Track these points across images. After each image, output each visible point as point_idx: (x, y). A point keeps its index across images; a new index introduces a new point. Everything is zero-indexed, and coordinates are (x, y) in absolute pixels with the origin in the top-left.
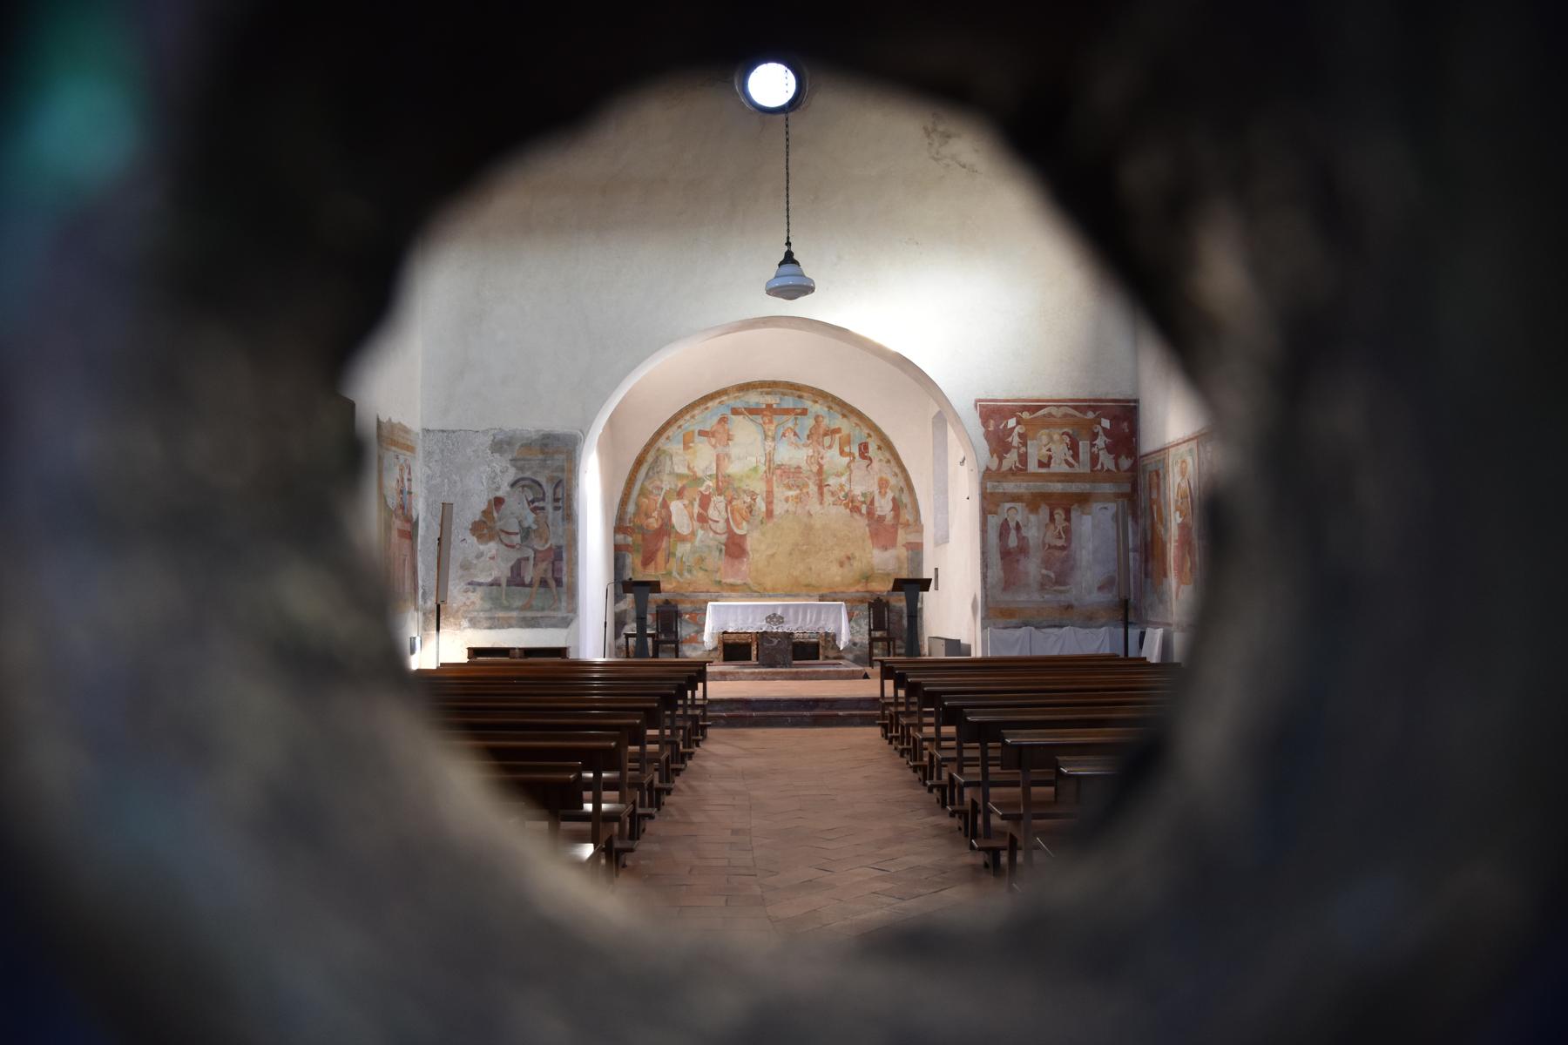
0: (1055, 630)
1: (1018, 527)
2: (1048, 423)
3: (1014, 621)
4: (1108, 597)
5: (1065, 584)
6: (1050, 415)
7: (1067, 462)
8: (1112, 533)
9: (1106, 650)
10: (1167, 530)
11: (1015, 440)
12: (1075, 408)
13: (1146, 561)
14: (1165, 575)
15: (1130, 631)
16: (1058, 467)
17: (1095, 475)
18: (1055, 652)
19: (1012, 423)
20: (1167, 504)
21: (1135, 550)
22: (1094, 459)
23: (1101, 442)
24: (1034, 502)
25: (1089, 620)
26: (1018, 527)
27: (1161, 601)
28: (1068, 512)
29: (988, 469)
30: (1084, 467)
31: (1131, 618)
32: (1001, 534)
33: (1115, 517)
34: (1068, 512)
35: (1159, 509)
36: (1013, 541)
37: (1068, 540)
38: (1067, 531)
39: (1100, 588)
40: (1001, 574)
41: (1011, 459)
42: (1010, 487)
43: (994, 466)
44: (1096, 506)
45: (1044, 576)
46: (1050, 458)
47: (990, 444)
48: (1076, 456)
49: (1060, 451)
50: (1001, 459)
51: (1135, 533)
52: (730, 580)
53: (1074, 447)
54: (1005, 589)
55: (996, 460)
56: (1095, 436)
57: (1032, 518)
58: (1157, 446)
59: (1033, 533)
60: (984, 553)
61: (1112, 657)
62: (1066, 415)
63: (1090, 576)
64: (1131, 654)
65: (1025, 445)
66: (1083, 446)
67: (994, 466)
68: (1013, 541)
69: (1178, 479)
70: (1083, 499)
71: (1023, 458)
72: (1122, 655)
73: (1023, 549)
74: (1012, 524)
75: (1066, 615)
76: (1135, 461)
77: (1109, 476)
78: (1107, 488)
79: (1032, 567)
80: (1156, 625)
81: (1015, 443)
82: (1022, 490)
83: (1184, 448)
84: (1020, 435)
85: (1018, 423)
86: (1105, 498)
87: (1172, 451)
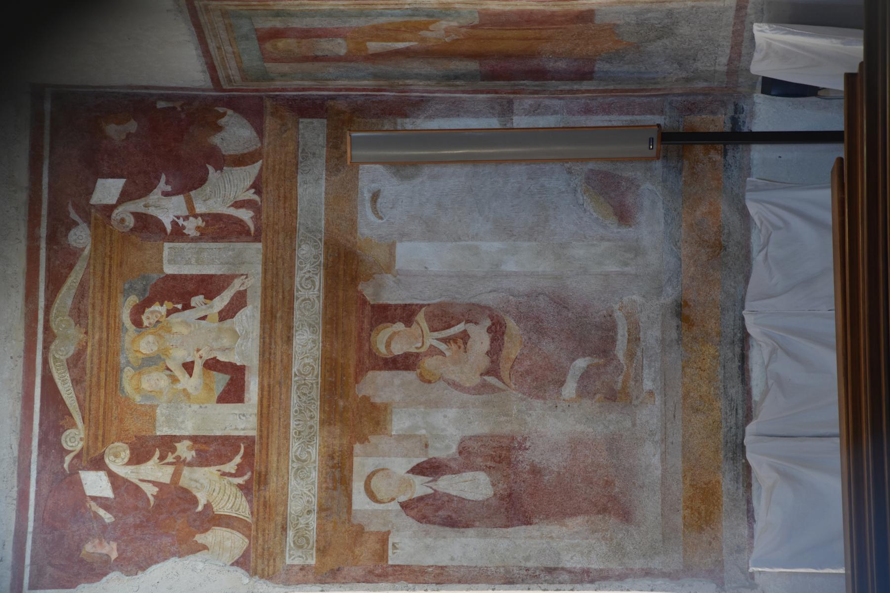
0: (757, 359)
1: (430, 469)
2: (99, 372)
3: (727, 484)
4: (651, 191)
5: (608, 331)
6: (75, 362)
7: (226, 314)
8: (453, 179)
9: (822, 200)
11: (153, 474)
12: (55, 283)
13: (540, 75)
15: (758, 126)
16: (242, 340)
17: (269, 226)
18: (828, 359)
19: (96, 484)
21: (507, 110)
22: (220, 228)
23: (167, 208)
24: (350, 416)
25: (724, 253)
26: (430, 469)
27: (667, 28)
28: (384, 314)
29: (242, 562)
30: (248, 262)
31: (720, 122)
32: (451, 523)
33: (402, 168)
34: (384, 314)
35: (378, 33)
36: (474, 486)
37: (472, 313)
38: (443, 317)
39: (624, 216)
40: (576, 523)
41: (213, 487)
42: (301, 490)
43: (232, 542)
44: (369, 227)
45: (583, 392)
46: (212, 365)
47: (162, 556)
48: (209, 286)
49: (191, 333)
50: (211, 519)
51: (455, 109)
52: (452, 377)
53: (181, 292)
54: (626, 516)
55: (214, 536)
56: (147, 225)
57: (399, 423)
59: (450, 424)
60: (182, 89)
61: (844, 178)
62: (78, 314)
63: (591, 250)
64: (836, 121)
65: (168, 443)
66: (178, 261)
67: (232, 542)
68: (474, 486)
70: (346, 266)
71: (212, 449)
72: (839, 151)
73: (499, 454)
74: (420, 486)
75: (707, 323)
76: (235, 104)
77: (276, 186)
78: (312, 191)
79: (555, 427)
80: (742, 43)
81: (164, 474)
82: (314, 453)
84: (139, 457)
85: (98, 464)
86: (343, 197)
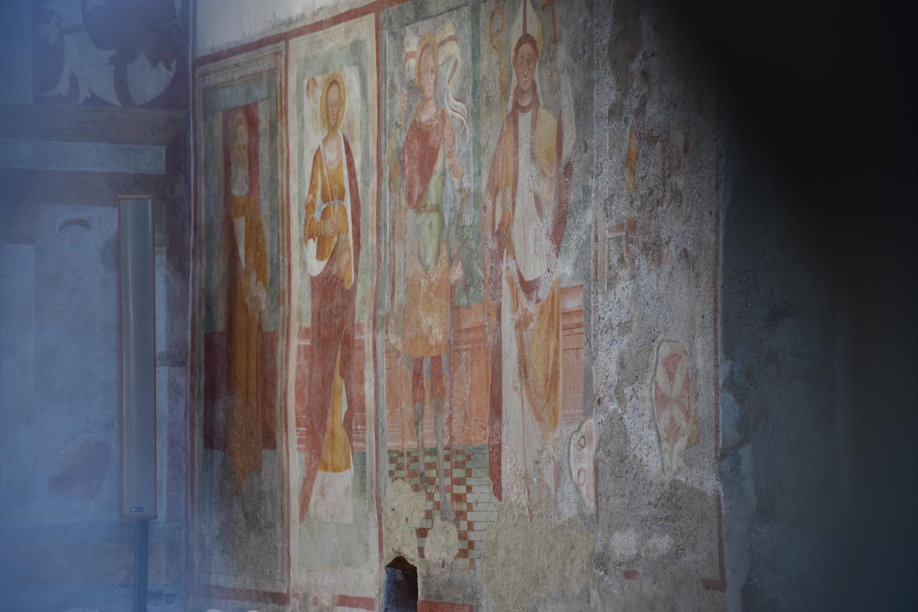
10: (280, 297)
14: (269, 440)
20: (281, 214)
21: (175, 360)
33: (114, 252)
35: (254, 228)
51: (176, 306)
58: (254, 27)
60: (195, 26)
69: (315, 137)
78: (93, 159)
83: (335, 39)
87: (299, 47)
